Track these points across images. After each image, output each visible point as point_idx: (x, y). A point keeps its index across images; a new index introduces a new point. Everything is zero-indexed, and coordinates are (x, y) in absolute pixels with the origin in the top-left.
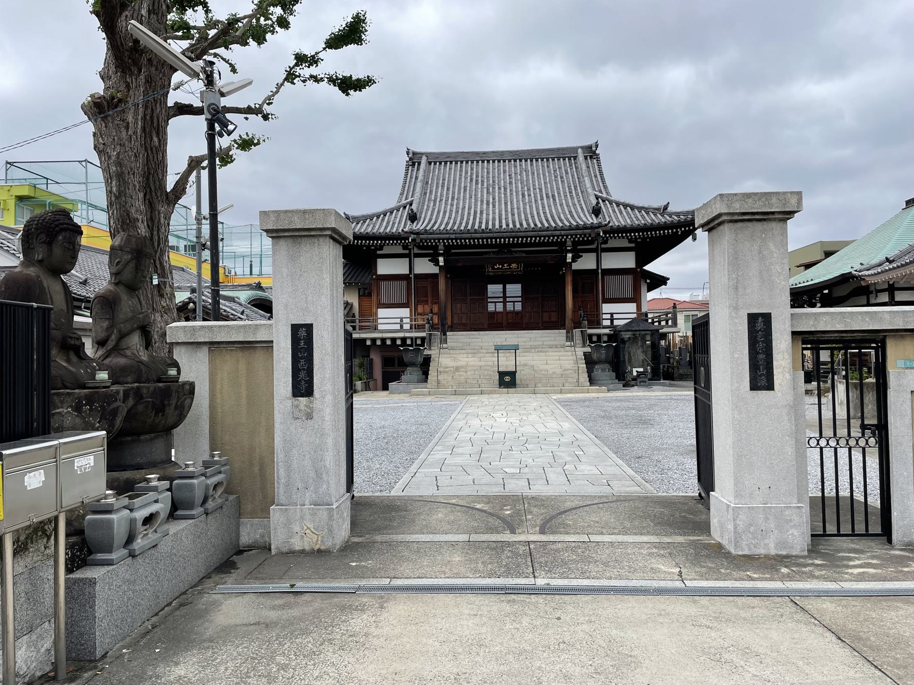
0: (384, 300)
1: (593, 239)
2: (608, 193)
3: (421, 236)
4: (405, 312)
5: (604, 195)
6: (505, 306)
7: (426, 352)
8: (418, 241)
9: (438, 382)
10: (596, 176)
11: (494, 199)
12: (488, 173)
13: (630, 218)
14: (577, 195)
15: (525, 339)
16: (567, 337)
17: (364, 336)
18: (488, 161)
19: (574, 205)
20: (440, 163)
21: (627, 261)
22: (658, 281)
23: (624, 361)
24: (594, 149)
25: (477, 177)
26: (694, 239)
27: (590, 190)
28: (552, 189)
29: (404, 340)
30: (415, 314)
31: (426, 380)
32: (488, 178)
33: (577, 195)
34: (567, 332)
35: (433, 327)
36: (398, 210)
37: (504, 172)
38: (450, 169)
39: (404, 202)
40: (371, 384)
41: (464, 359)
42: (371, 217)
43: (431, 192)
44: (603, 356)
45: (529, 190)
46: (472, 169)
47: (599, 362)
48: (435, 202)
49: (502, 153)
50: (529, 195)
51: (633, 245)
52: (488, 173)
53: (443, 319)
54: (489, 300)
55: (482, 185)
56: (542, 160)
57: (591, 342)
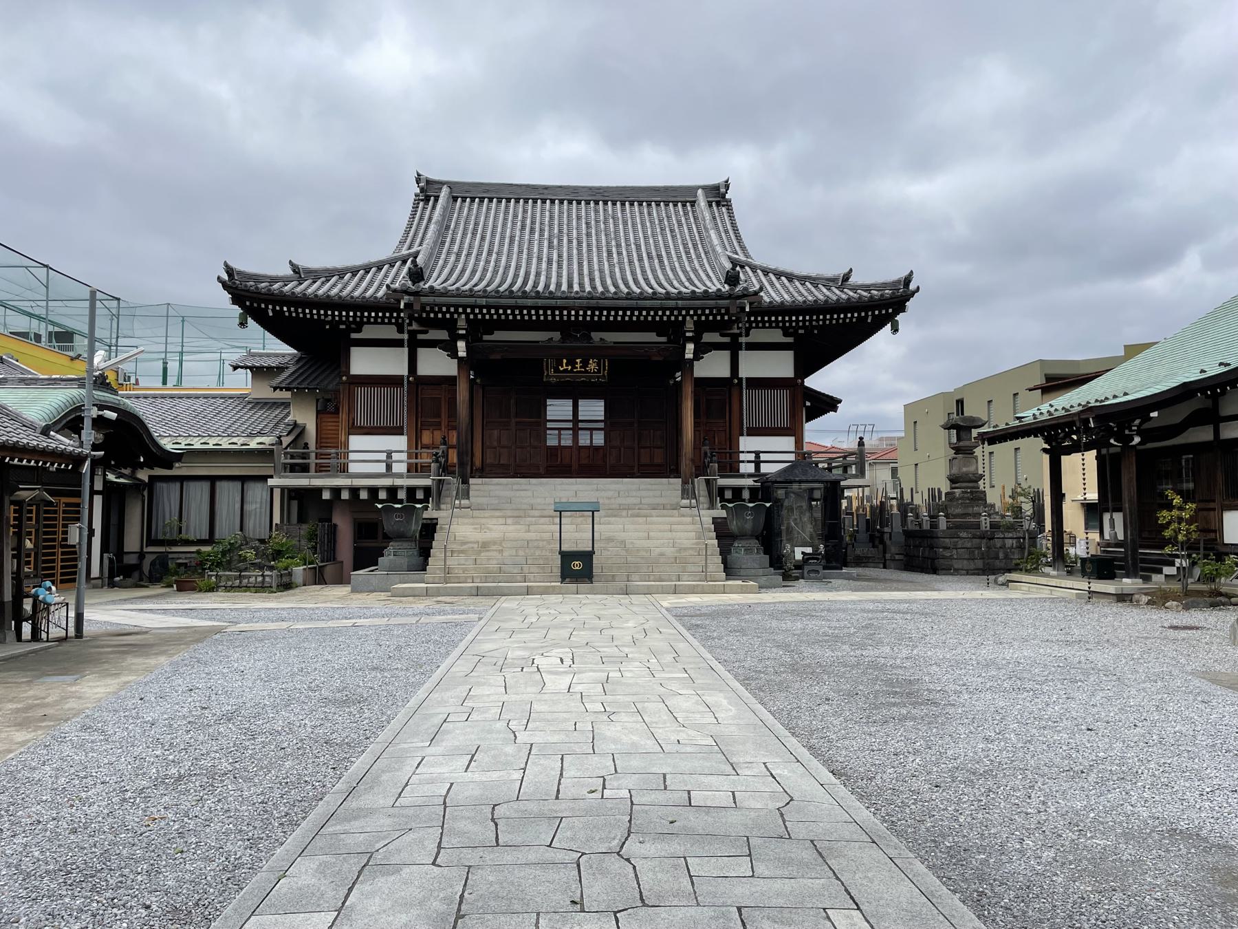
0: (361, 421)
1: (732, 315)
2: (747, 255)
3: (424, 299)
4: (399, 443)
5: (742, 257)
6: (575, 438)
7: (430, 513)
8: (417, 307)
9: (447, 571)
10: (726, 232)
11: (560, 256)
12: (551, 218)
13: (788, 292)
14: (699, 256)
15: (610, 494)
16: (684, 491)
17: (317, 482)
18: (553, 202)
19: (695, 271)
20: (473, 199)
21: (780, 365)
22: (826, 404)
23: (780, 534)
24: (723, 190)
25: (533, 223)
26: (895, 330)
27: (719, 249)
28: (657, 246)
29: (392, 491)
30: (416, 444)
31: (423, 567)
32: (551, 225)
33: (699, 256)
34: (685, 483)
35: (446, 469)
36: (392, 266)
37: (579, 218)
38: (488, 209)
39: (405, 252)
40: (329, 570)
41: (496, 528)
42: (341, 273)
43: (453, 241)
44: (749, 526)
45: (618, 246)
46: (525, 211)
47: (742, 536)
48: (458, 255)
49: (575, 190)
50: (619, 254)
51: (790, 340)
52: (551, 218)
53: (465, 453)
54: (549, 425)
55: (541, 235)
56: (640, 204)
57: (723, 499)
